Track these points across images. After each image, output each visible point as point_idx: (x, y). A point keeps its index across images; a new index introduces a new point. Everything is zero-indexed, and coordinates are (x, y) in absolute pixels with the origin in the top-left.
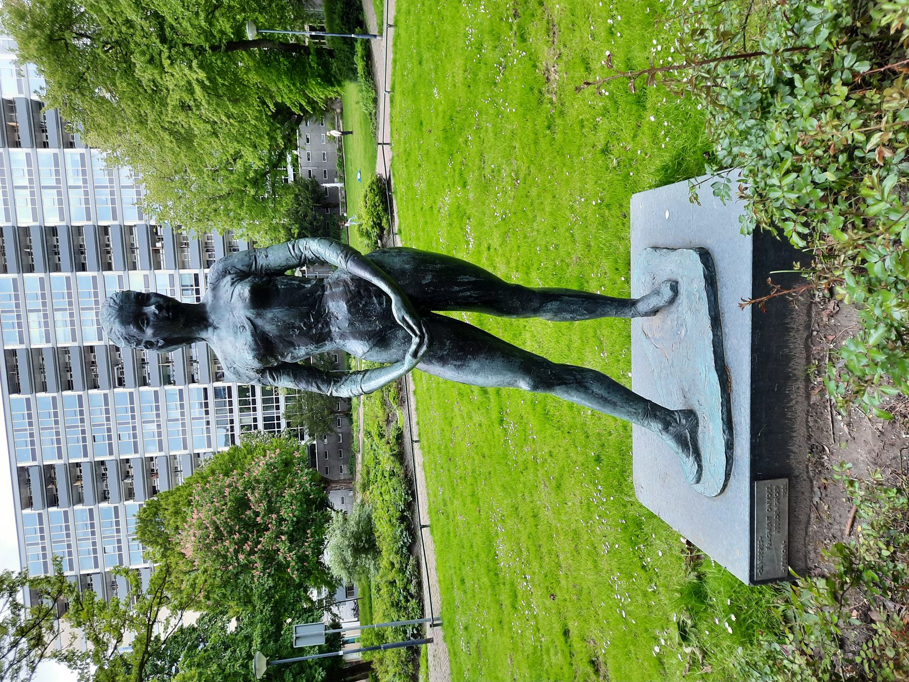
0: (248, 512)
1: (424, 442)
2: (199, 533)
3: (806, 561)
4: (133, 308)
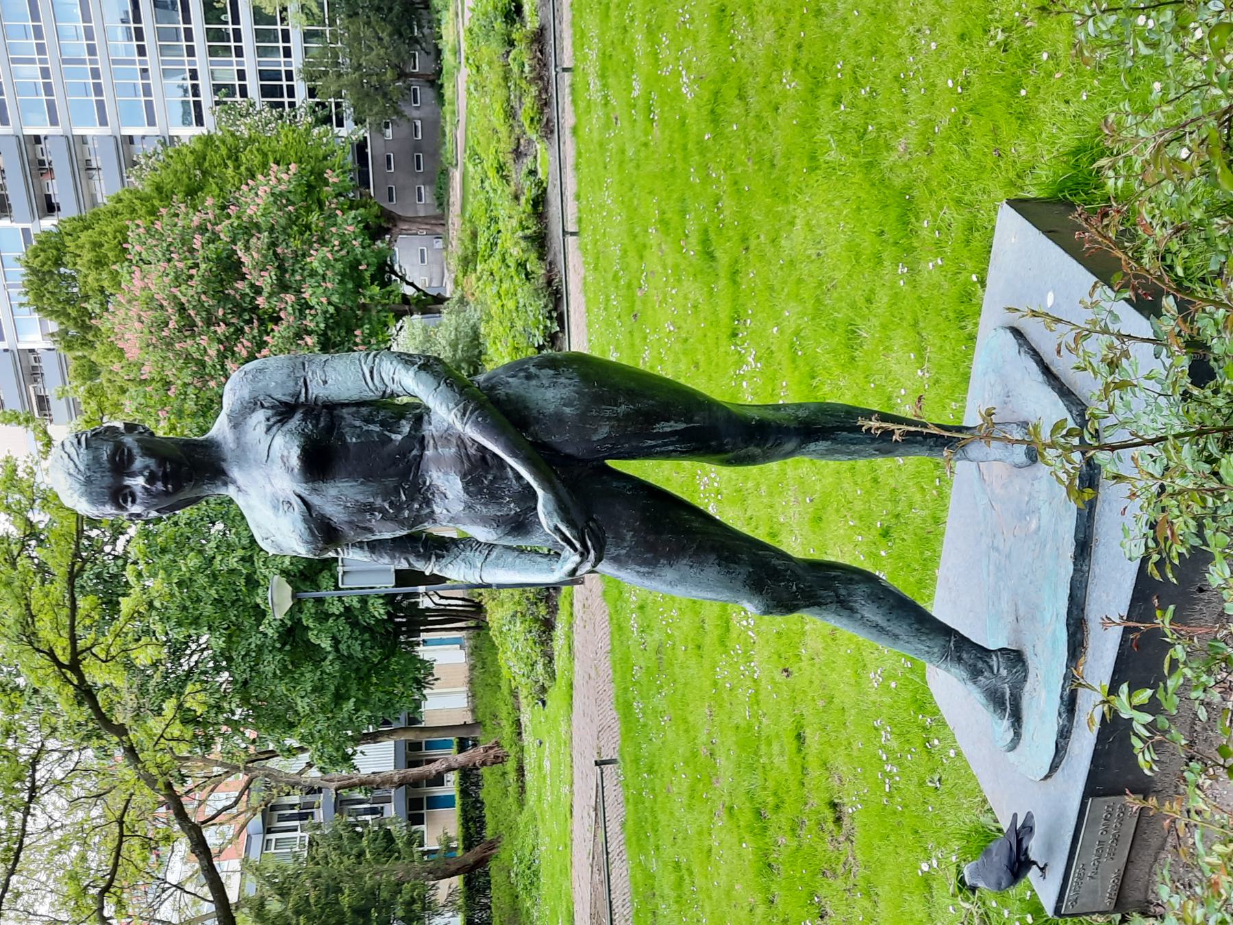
0: (239, 285)
1: (587, 237)
2: (149, 316)
3: (1147, 891)
4: (108, 480)
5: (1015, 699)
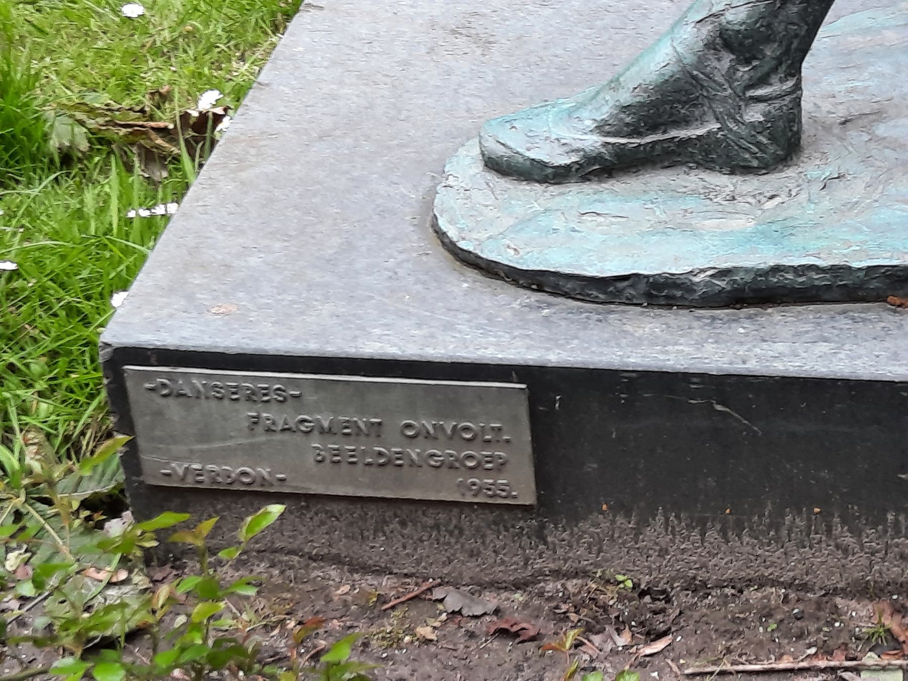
5: (668, 153)
